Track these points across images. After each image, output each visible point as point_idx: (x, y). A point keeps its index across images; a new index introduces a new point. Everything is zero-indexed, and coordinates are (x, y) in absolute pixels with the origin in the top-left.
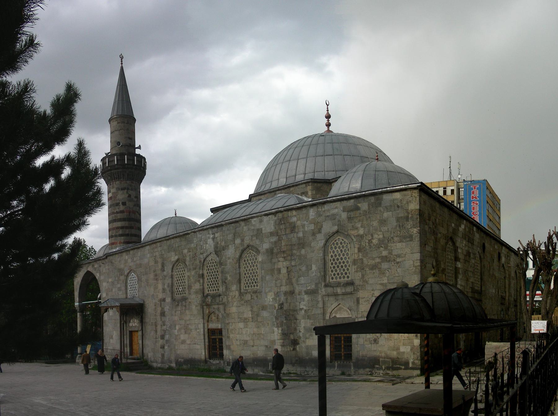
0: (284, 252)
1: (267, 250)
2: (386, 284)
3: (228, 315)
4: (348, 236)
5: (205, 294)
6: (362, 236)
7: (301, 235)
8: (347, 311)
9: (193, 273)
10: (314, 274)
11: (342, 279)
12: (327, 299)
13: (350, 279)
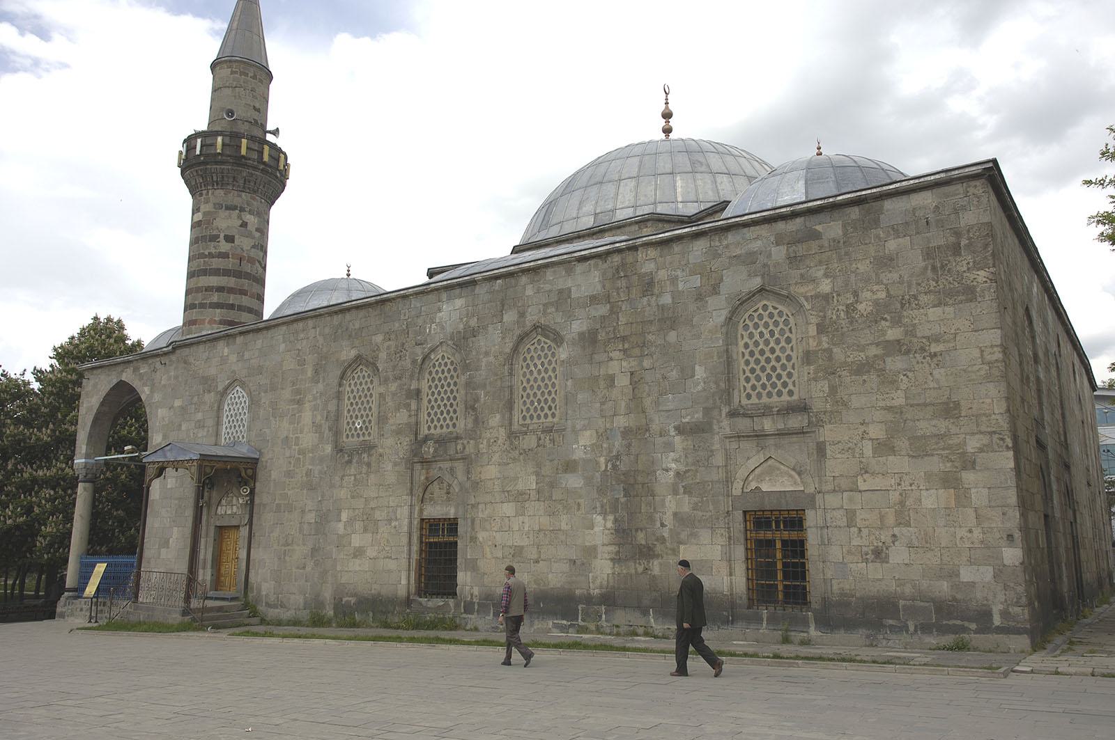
0: (624, 339)
1: (581, 335)
2: (901, 407)
3: (476, 485)
4: (789, 299)
5: (420, 437)
6: (827, 298)
7: (667, 299)
8: (791, 476)
9: (393, 387)
10: (700, 388)
11: (775, 398)
12: (734, 445)
13: (795, 397)
